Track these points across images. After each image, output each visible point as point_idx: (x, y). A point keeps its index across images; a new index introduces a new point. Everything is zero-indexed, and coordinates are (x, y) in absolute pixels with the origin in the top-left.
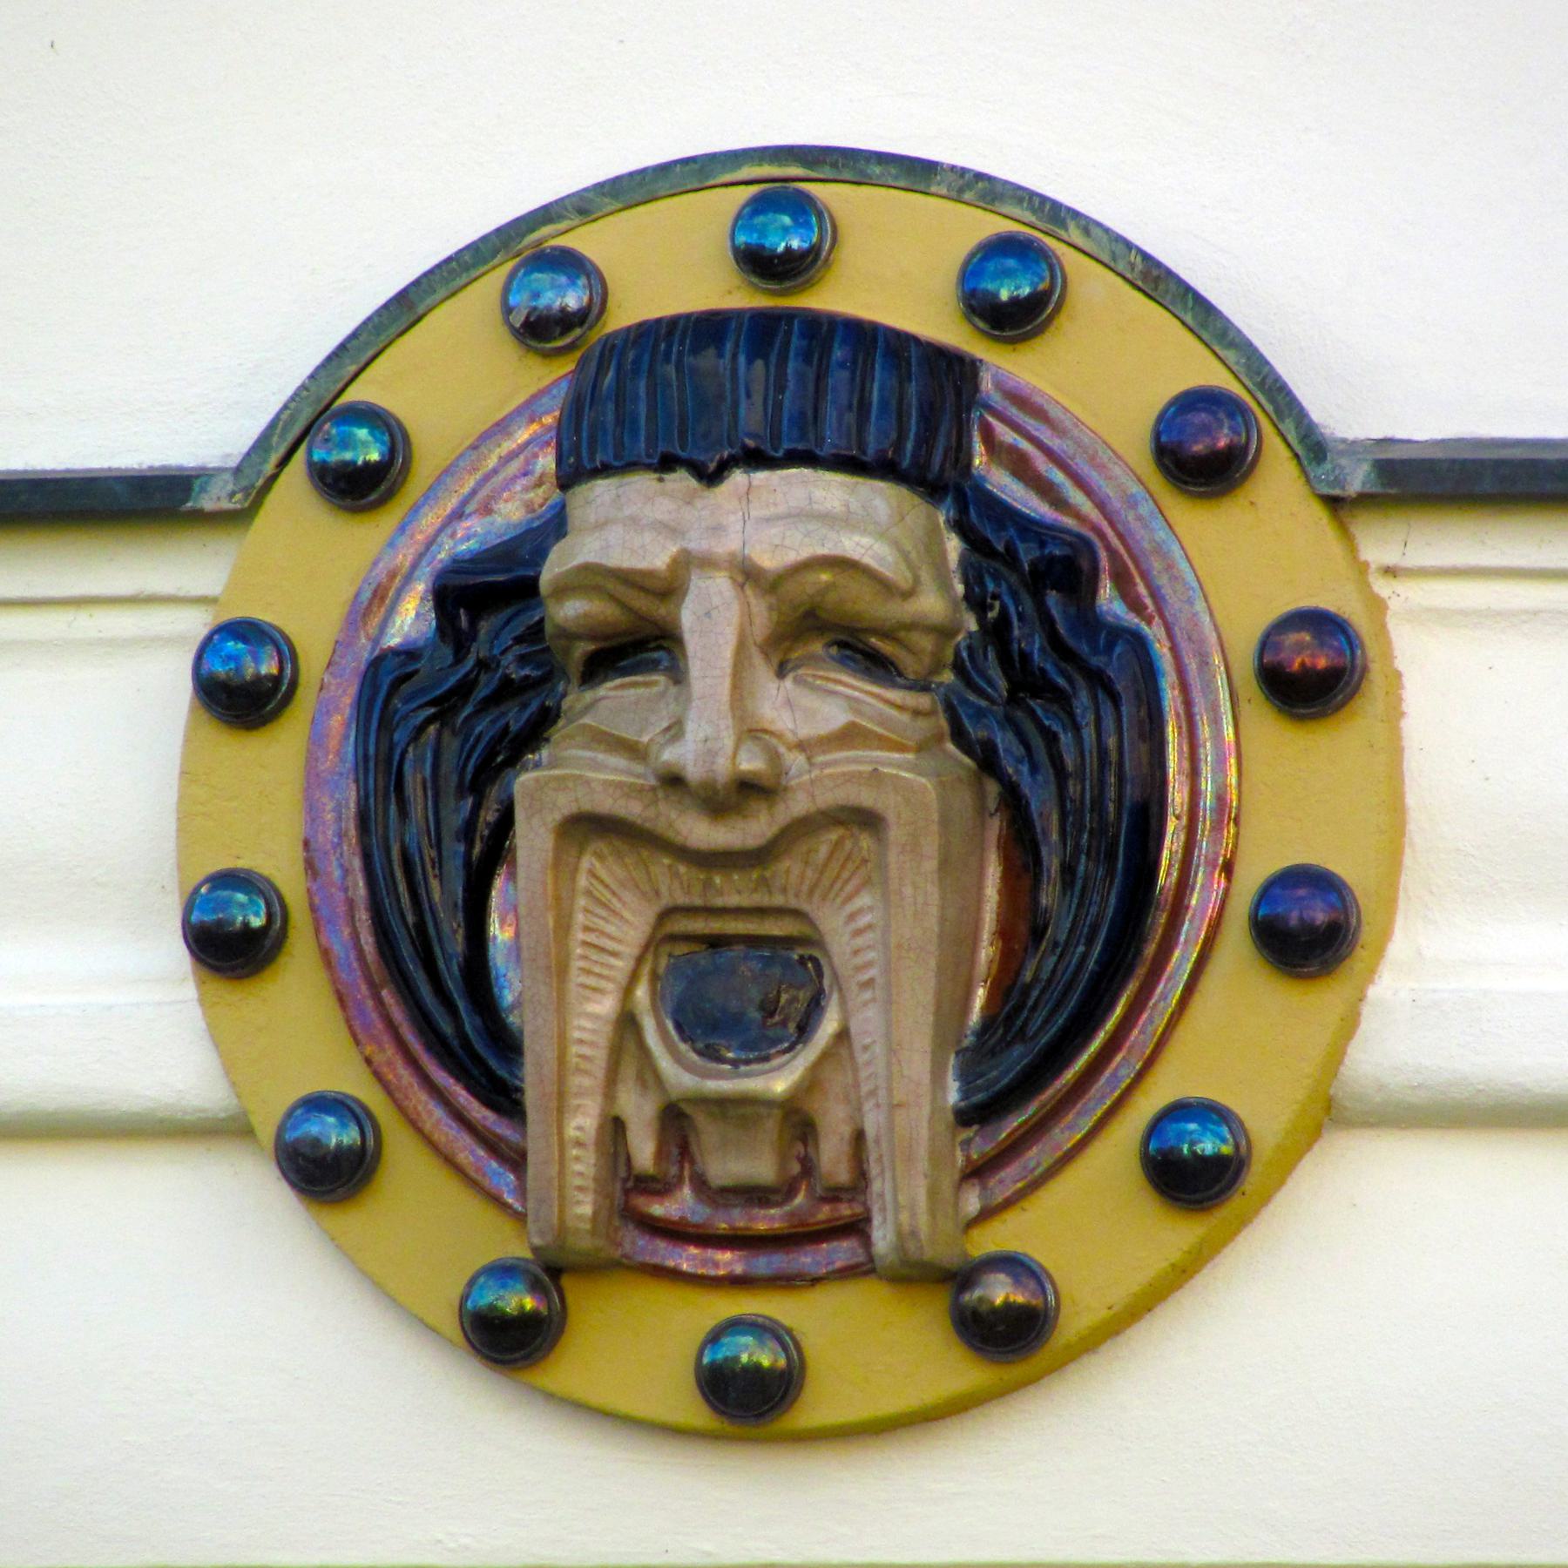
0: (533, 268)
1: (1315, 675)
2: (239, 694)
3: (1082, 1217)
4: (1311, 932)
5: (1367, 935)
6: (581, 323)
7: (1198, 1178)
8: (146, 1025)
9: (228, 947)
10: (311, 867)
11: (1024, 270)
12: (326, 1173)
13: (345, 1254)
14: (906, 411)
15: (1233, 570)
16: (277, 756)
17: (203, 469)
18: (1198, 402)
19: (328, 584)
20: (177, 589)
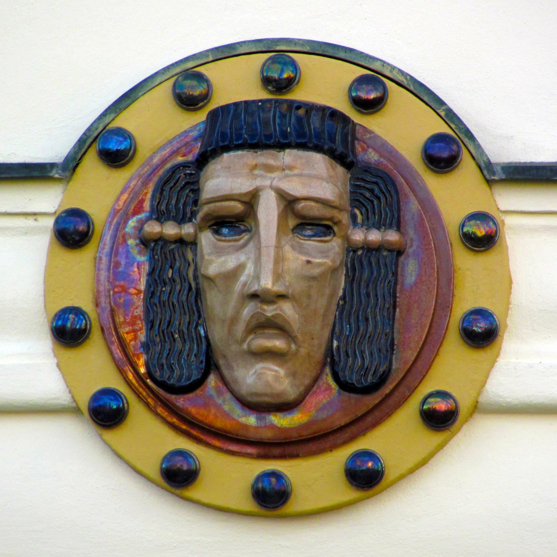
0: (187, 85)
1: (483, 239)
2: (72, 232)
3: (394, 438)
4: (482, 334)
5: (500, 333)
6: (202, 100)
7: (441, 420)
8: (32, 366)
9: (68, 332)
10: (97, 305)
11: (374, 86)
12: (106, 414)
13: (406, 400)
14: (328, 134)
15: (455, 197)
16: (82, 261)
17: (75, 175)
18: (439, 138)
19: (100, 192)
20: (47, 200)
